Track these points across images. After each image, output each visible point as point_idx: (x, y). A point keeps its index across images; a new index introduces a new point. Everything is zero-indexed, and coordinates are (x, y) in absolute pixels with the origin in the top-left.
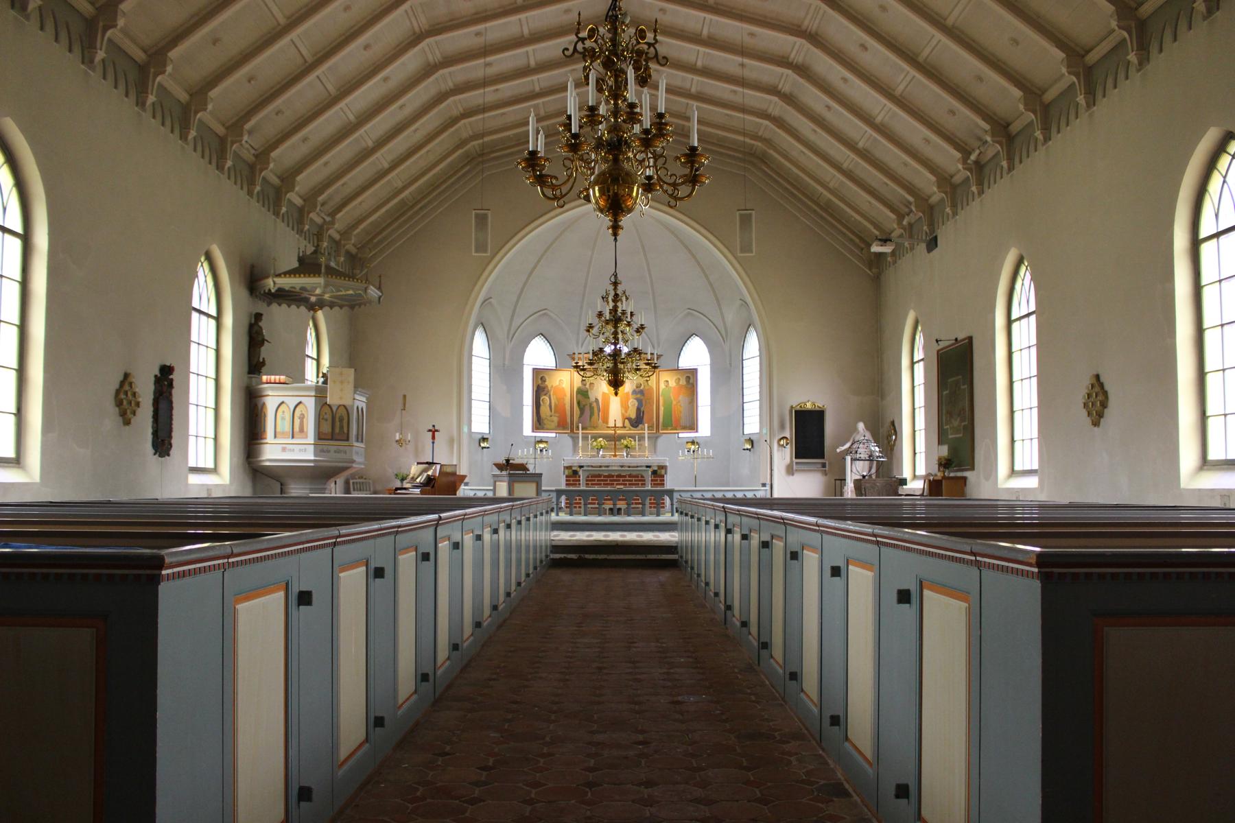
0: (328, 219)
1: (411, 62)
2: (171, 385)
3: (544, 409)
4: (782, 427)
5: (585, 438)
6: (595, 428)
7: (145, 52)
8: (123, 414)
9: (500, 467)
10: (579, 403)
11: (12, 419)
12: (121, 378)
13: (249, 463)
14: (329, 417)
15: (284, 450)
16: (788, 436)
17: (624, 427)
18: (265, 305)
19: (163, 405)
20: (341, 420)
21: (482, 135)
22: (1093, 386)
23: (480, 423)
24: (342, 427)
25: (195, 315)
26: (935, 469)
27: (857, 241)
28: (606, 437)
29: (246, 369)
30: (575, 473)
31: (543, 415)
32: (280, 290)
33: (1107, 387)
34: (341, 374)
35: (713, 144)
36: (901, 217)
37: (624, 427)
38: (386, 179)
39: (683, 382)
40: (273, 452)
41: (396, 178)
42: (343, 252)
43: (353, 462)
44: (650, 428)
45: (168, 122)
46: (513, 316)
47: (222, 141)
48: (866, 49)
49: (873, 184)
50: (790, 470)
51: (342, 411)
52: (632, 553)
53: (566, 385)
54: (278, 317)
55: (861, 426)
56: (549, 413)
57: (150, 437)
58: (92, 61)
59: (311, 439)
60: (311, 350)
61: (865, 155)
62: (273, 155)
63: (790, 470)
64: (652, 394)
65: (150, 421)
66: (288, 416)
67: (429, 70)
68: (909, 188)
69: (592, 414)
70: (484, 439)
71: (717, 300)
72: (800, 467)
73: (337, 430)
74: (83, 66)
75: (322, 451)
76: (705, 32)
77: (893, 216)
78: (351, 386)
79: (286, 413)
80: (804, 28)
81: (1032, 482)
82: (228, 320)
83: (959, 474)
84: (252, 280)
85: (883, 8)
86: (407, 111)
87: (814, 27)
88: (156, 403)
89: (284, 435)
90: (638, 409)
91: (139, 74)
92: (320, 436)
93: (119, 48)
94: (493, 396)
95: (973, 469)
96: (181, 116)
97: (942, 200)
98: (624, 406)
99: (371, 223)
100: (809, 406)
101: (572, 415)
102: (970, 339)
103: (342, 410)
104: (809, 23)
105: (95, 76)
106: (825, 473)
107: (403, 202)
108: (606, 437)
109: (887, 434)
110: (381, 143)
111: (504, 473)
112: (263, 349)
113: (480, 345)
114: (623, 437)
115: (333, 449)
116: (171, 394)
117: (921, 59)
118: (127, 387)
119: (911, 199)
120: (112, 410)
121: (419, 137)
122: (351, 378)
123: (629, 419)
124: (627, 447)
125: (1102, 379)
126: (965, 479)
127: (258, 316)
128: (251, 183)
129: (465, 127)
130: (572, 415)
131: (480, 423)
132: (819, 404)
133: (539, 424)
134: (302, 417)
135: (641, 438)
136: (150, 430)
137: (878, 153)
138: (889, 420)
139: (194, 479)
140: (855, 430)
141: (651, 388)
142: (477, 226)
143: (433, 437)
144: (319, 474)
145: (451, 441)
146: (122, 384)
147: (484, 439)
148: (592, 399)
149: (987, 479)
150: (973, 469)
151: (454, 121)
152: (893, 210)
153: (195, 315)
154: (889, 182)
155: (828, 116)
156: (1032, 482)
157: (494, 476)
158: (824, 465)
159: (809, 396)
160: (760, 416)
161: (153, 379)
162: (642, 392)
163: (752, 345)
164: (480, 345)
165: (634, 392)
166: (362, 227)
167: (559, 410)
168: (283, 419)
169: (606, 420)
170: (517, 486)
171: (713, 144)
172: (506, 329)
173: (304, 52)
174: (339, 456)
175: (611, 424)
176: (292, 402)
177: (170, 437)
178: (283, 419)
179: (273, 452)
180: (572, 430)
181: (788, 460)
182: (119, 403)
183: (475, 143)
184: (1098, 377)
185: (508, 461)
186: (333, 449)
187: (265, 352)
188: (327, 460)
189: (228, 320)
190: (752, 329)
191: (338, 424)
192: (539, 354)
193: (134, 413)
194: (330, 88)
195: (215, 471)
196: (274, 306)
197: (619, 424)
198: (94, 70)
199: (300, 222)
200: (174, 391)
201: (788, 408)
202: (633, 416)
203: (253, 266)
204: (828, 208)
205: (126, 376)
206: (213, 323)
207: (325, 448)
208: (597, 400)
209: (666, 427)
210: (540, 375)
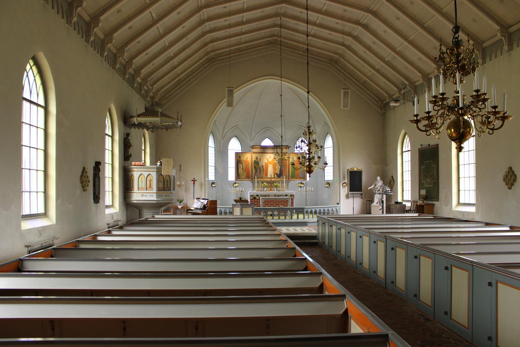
0: (151, 88)
1: (195, 19)
2: (99, 170)
3: (240, 170)
4: (344, 178)
5: (258, 182)
6: (262, 178)
7: (89, 16)
8: (83, 187)
9: (236, 201)
10: (255, 167)
12: (82, 170)
13: (125, 201)
14: (162, 180)
15: (142, 195)
17: (274, 178)
18: (129, 129)
19: (97, 180)
20: (167, 181)
21: (215, 50)
22: (509, 172)
23: (212, 177)
25: (26, 104)
26: (417, 198)
27: (376, 98)
28: (267, 182)
29: (123, 158)
30: (255, 198)
31: (240, 172)
32: (139, 123)
33: (516, 173)
34: (168, 161)
35: (314, 55)
36: (400, 90)
37: (274, 178)
38: (175, 71)
40: (137, 197)
41: (179, 70)
43: (172, 200)
44: (286, 178)
45: (96, 49)
46: (224, 128)
47: (115, 55)
48: (399, 19)
49: (389, 75)
50: (347, 197)
51: (168, 178)
52: (299, 239)
53: (249, 159)
54: (134, 132)
55: (379, 178)
57: (92, 195)
58: (71, 23)
59: (155, 190)
60: (108, 131)
61: (388, 63)
62: (134, 61)
63: (347, 197)
65: (92, 187)
66: (144, 180)
67: (202, 22)
68: (407, 78)
69: (260, 172)
70: (213, 183)
73: (166, 186)
74: (67, 25)
75: (160, 196)
76: (324, 9)
77: (396, 89)
78: (172, 166)
80: (370, 9)
81: (472, 209)
83: (430, 202)
84: (126, 119)
85: (412, 3)
87: (375, 9)
89: (142, 189)
90: (280, 170)
91: (86, 28)
92: (159, 189)
93: (82, 17)
94: (219, 163)
95: (438, 201)
97: (423, 84)
98: (274, 168)
100: (355, 169)
102: (438, 145)
103: (168, 178)
104: (374, 7)
105: (71, 29)
106: (362, 198)
107: (180, 79)
108: (267, 182)
109: (391, 182)
110: (176, 55)
111: (238, 203)
113: (211, 143)
115: (164, 195)
117: (425, 25)
118: (85, 174)
119: (407, 83)
120: (79, 185)
122: (172, 163)
124: (276, 186)
125: (513, 169)
126: (433, 205)
127: (128, 135)
128: (124, 74)
129: (210, 47)
131: (212, 177)
133: (238, 176)
134: (150, 181)
135: (282, 182)
136: (92, 192)
137: (394, 63)
138: (390, 176)
140: (376, 179)
142: (228, 93)
143: (194, 184)
144: (156, 207)
146: (83, 172)
147: (213, 183)
148: (261, 165)
149: (446, 205)
150: (438, 201)
151: (206, 44)
152: (396, 86)
153: (26, 104)
154: (396, 74)
155: (374, 47)
156: (472, 209)
157: (233, 205)
158: (362, 194)
159: (355, 164)
160: (334, 172)
161: (93, 168)
163: (329, 143)
164: (211, 143)
166: (162, 90)
167: (246, 170)
168: (142, 181)
169: (266, 175)
170: (245, 210)
171: (314, 55)
172: (221, 134)
173: (154, 15)
175: (269, 176)
176: (146, 174)
177: (99, 194)
178: (142, 181)
179: (137, 197)
180: (252, 179)
181: (346, 192)
182: (82, 182)
183: (212, 54)
184: (511, 168)
185: (240, 198)
187: (131, 151)
188: (161, 200)
189: (117, 137)
190: (329, 135)
191: (166, 183)
192: (234, 146)
194: (161, 31)
196: (133, 129)
197: (272, 176)
198: (71, 26)
199: (140, 90)
200: (100, 173)
201: (347, 170)
202: (278, 173)
203: (125, 112)
204: (364, 84)
205: (84, 168)
206: (42, 111)
207: (161, 194)
208: (262, 166)
209: (292, 178)
210: (238, 156)
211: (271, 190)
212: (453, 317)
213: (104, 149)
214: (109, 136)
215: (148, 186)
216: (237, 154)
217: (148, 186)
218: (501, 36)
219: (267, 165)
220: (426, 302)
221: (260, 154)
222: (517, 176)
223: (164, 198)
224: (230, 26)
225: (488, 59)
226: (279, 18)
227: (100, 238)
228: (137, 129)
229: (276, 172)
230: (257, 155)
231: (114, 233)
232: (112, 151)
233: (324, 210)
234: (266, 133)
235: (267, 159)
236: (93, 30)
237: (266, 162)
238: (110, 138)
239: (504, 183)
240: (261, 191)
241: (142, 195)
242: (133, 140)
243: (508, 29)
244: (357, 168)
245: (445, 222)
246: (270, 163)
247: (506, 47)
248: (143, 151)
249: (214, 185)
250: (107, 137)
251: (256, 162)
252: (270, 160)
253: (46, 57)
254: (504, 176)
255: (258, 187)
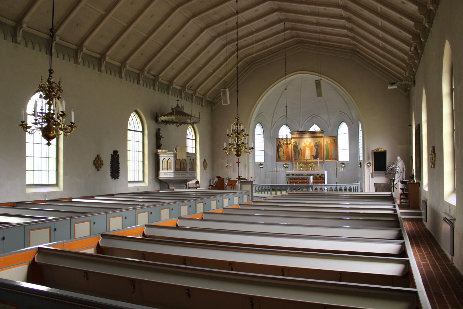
3: (281, 153)
4: (369, 158)
5: (296, 163)
6: (300, 159)
10: (294, 150)
11: (55, 172)
12: (96, 156)
14: (179, 163)
15: (165, 174)
16: (371, 162)
20: (183, 163)
24: (184, 166)
25: (128, 131)
28: (303, 163)
29: (155, 147)
39: (333, 141)
41: (219, 74)
42: (204, 101)
47: (139, 74)
55: (399, 158)
56: (282, 154)
58: (77, 62)
64: (321, 146)
69: (299, 155)
70: (261, 164)
71: (349, 108)
72: (375, 175)
73: (182, 167)
75: (177, 174)
79: (165, 162)
82: (146, 132)
84: (155, 117)
86: (212, 53)
88: (112, 163)
89: (165, 169)
90: (316, 152)
92: (176, 169)
96: (119, 70)
98: (311, 151)
99: (214, 90)
100: (380, 150)
101: (292, 155)
106: (387, 177)
108: (303, 163)
112: (161, 140)
113: (259, 130)
114: (309, 163)
115: (181, 173)
116: (118, 159)
121: (222, 59)
123: (313, 156)
127: (159, 130)
130: (292, 155)
132: (384, 149)
134: (170, 163)
135: (317, 163)
136: (110, 171)
139: (130, 185)
141: (321, 144)
143: (238, 165)
145: (245, 166)
147: (261, 164)
148: (299, 148)
159: (379, 146)
162: (318, 146)
164: (259, 130)
165: (315, 146)
167: (287, 154)
169: (304, 157)
174: (184, 176)
181: (371, 172)
183: (245, 59)
184: (98, 156)
186: (181, 173)
187: (162, 141)
189: (146, 132)
191: (182, 165)
193: (101, 168)
195: (143, 181)
197: (310, 158)
202: (314, 154)
206: (141, 134)
208: (301, 149)
209: (326, 159)
211: (307, 170)
215: (168, 167)
217: (182, 167)
219: (304, 148)
221: (299, 139)
223: (180, 176)
224: (318, 24)
226: (283, 23)
227: (74, 200)
228: (171, 125)
229: (312, 154)
230: (296, 140)
231: (96, 198)
233: (350, 187)
234: (313, 120)
235: (305, 143)
237: (304, 145)
240: (299, 170)
241: (165, 174)
242: (162, 133)
244: (381, 149)
245: (363, 200)
246: (307, 146)
249: (261, 166)
251: (296, 147)
252: (307, 144)
255: (296, 167)
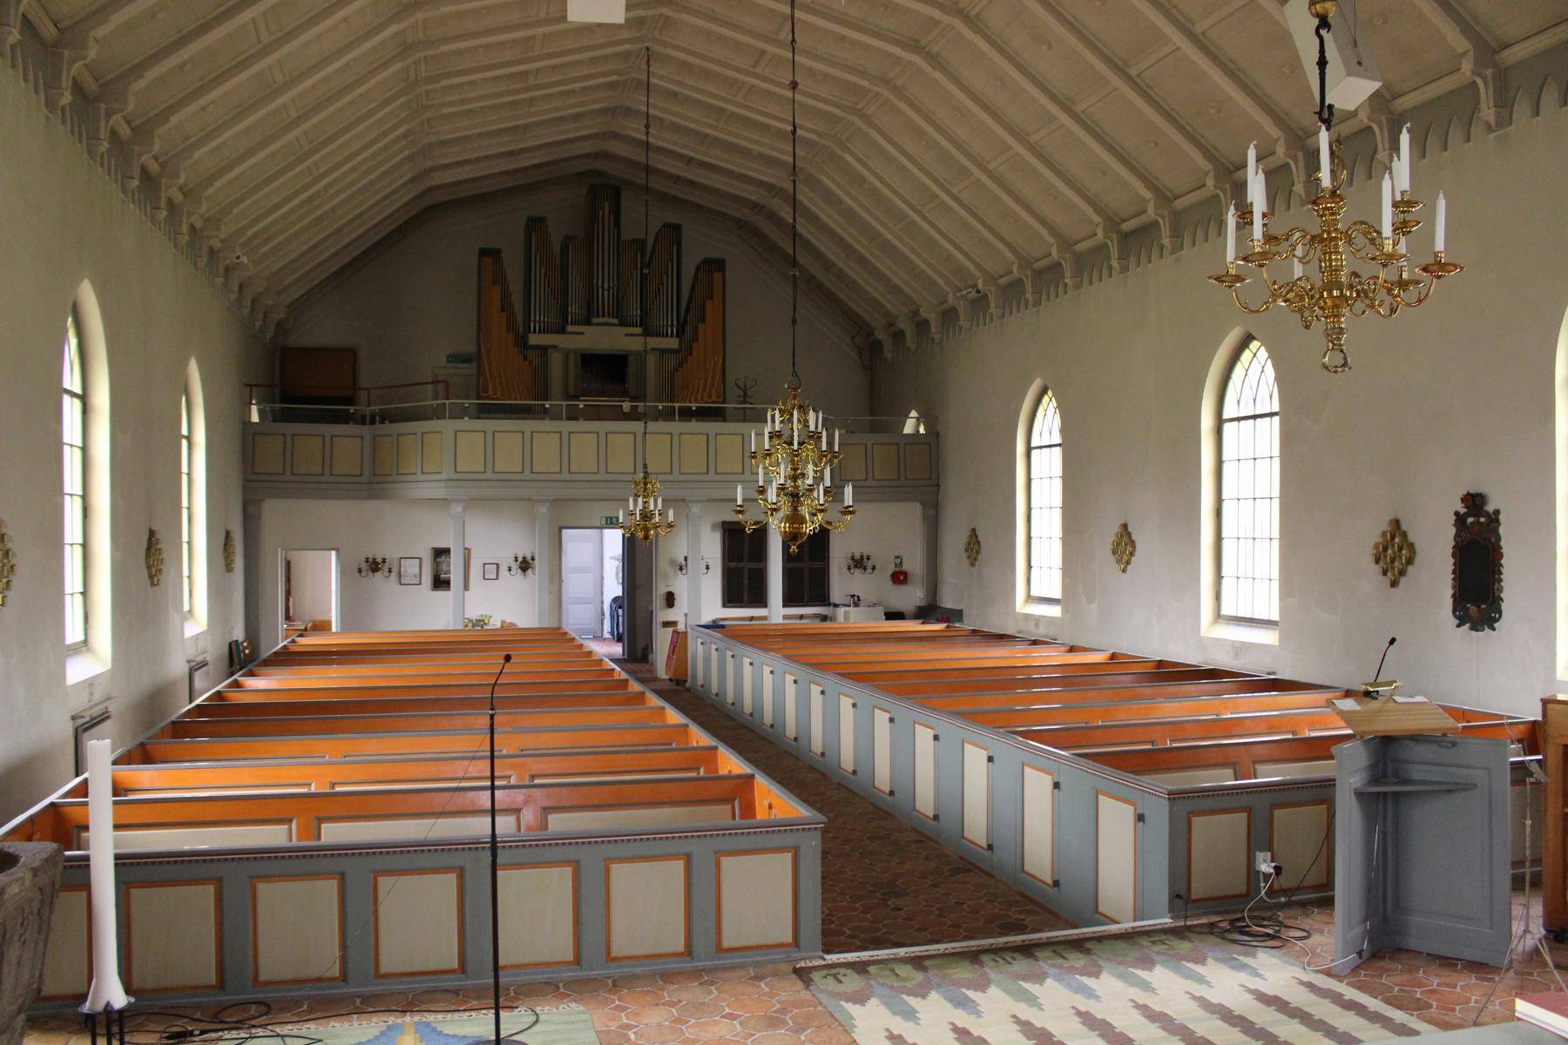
8: (151, 577)
12: (146, 536)
60: (72, 381)
125: (1404, 527)
184: (1396, 523)
205: (152, 533)
212: (1101, 909)
213: (59, 444)
214: (73, 395)
216: (704, 321)
218: (1370, 119)
220: (1038, 875)
222: (1418, 548)
225: (1522, 110)
232: (85, 450)
236: (69, 69)
238: (77, 403)
239: (1377, 569)
243: (1495, 52)
247: (1487, 112)
248: (184, 443)
250: (67, 399)
253: (95, 290)
254: (1376, 546)
